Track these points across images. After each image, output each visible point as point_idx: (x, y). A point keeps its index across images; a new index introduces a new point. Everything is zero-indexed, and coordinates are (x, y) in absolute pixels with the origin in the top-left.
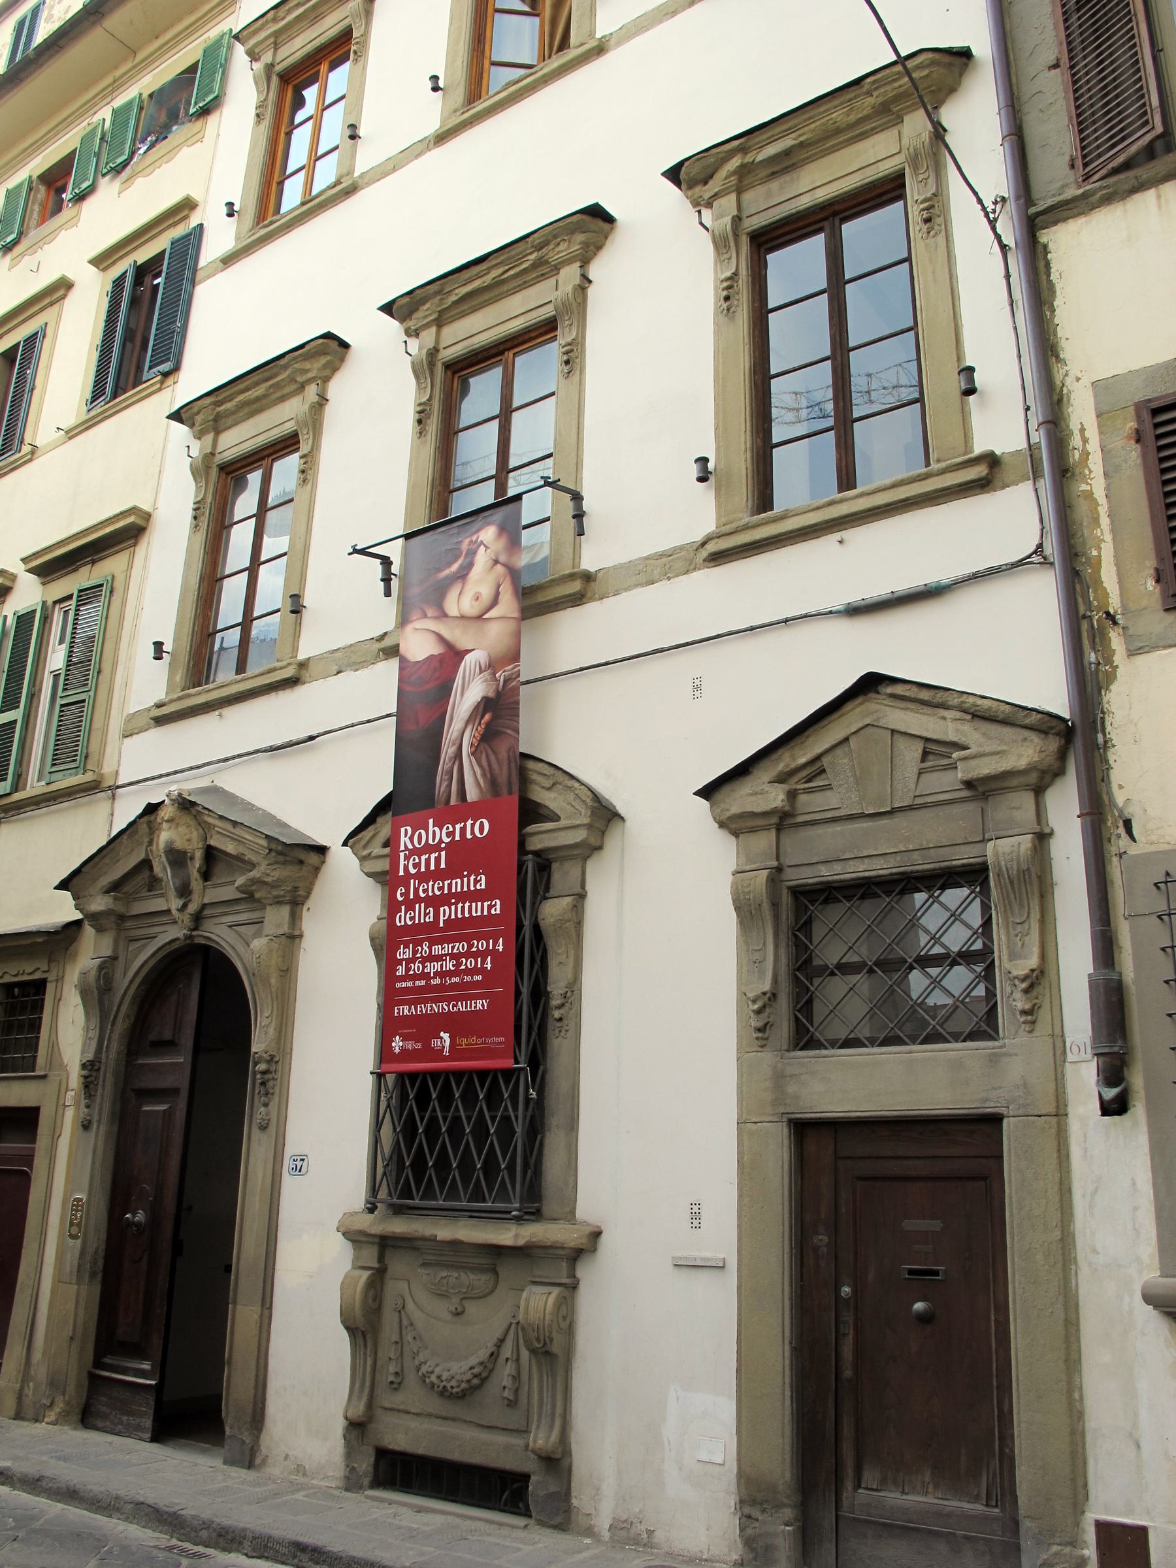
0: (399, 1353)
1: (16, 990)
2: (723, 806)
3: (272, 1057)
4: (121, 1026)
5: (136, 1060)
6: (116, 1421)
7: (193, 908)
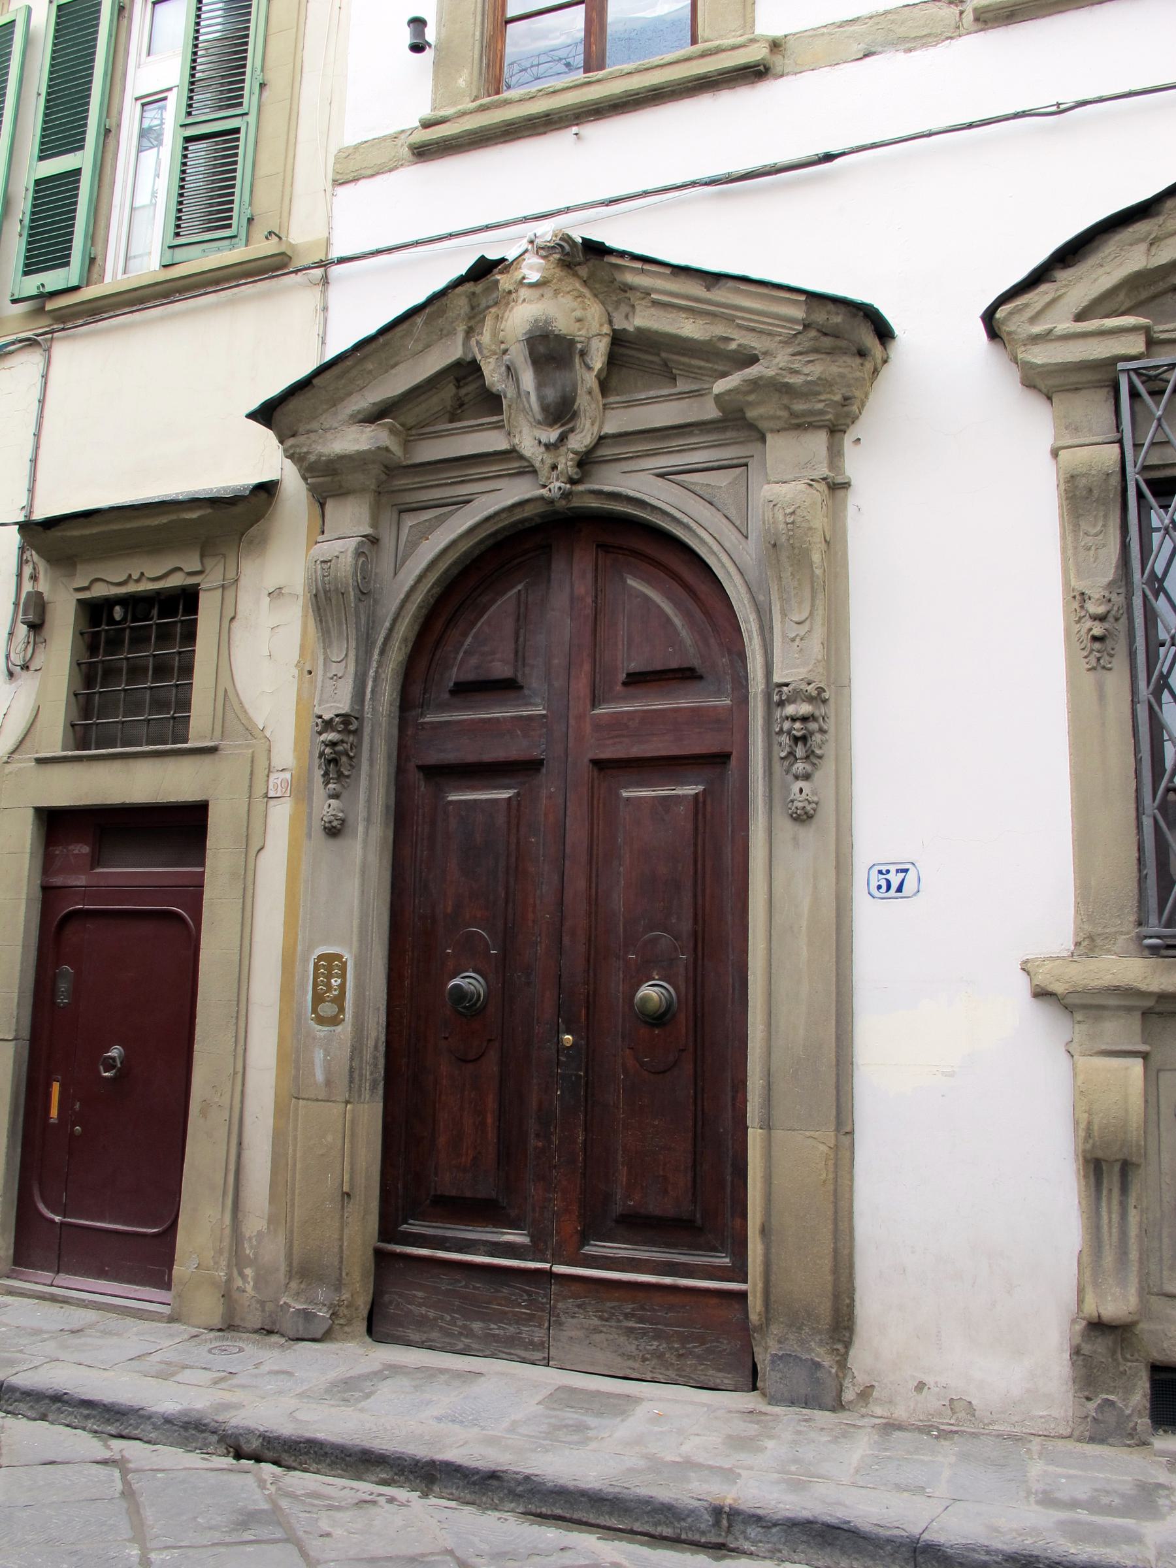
1: (118, 609)
3: (821, 690)
4: (397, 655)
5: (422, 715)
6: (456, 1330)
7: (580, 440)
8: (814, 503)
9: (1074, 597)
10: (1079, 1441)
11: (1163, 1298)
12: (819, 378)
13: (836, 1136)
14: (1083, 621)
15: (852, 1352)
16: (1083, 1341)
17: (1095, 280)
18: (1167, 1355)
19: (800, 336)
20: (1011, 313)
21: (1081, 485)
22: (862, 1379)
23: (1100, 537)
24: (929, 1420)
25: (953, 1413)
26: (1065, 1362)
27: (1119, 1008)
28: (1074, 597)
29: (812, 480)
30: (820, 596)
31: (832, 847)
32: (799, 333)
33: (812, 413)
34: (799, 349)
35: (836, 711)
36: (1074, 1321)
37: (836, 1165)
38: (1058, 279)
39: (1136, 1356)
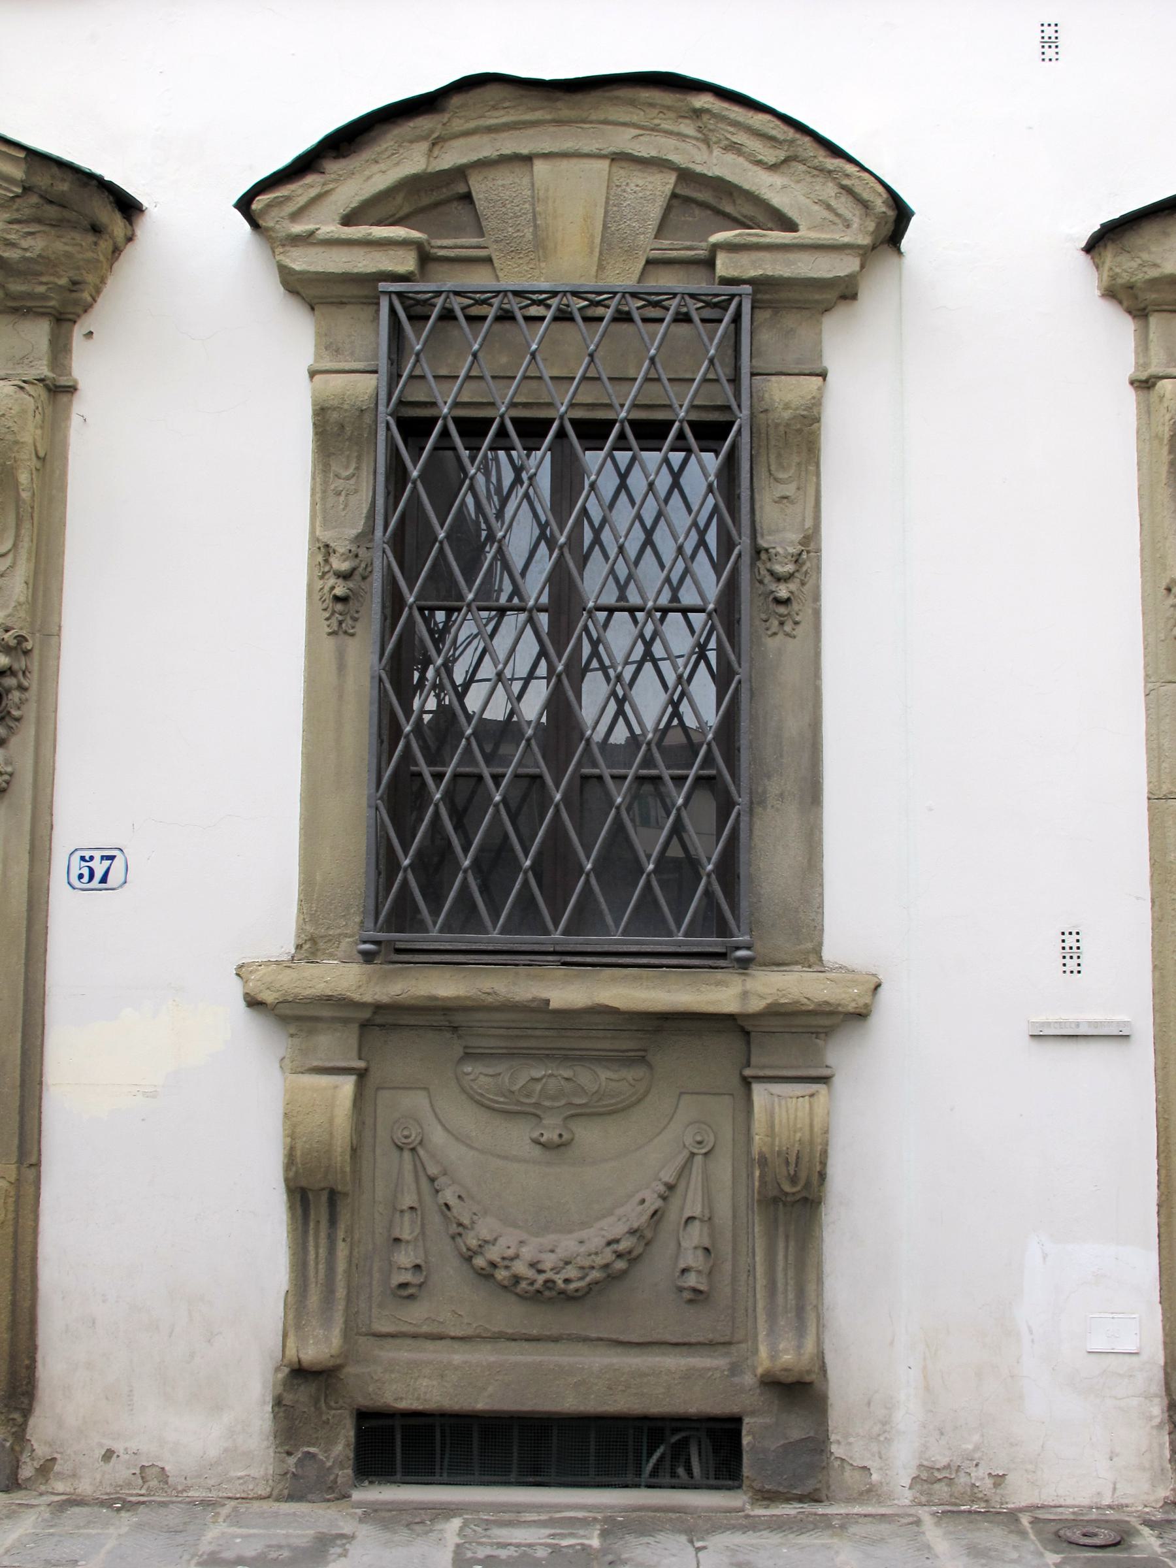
0: (417, 1231)
2: (1145, 256)
3: (21, 639)
8: (24, 411)
9: (319, 548)
10: (277, 1500)
11: (372, 1339)
12: (39, 256)
13: (18, 1169)
14: (326, 577)
15: (32, 1422)
16: (284, 1390)
17: (369, 178)
18: (372, 1399)
19: (18, 200)
20: (270, 206)
21: (332, 420)
22: (42, 1450)
23: (352, 481)
24: (117, 1493)
25: (144, 1482)
26: (267, 1415)
27: (333, 1020)
28: (319, 548)
29: (25, 382)
30: (27, 525)
31: (27, 827)
32: (17, 196)
33: (31, 296)
34: (17, 216)
35: (41, 664)
36: (277, 1369)
37: (17, 1203)
38: (327, 171)
39: (341, 1402)
